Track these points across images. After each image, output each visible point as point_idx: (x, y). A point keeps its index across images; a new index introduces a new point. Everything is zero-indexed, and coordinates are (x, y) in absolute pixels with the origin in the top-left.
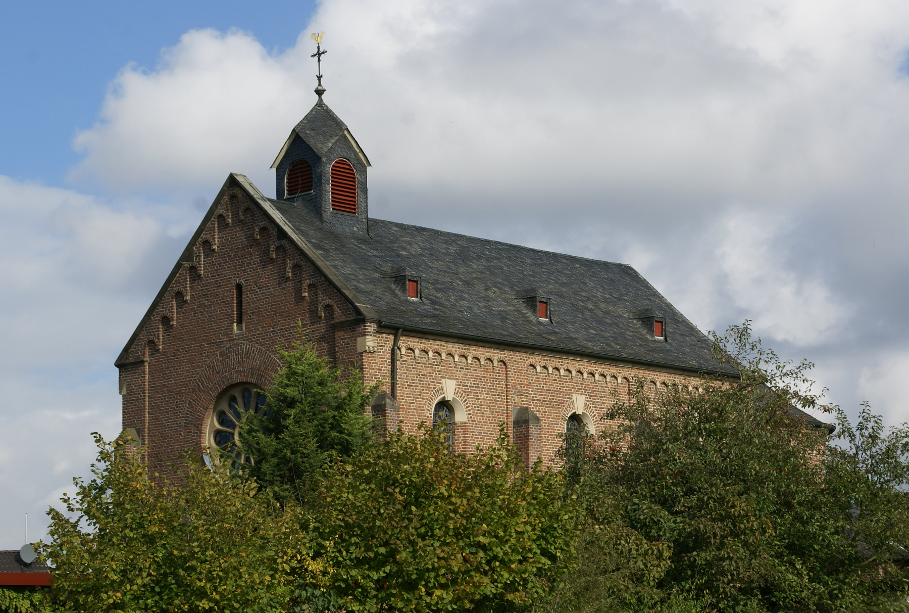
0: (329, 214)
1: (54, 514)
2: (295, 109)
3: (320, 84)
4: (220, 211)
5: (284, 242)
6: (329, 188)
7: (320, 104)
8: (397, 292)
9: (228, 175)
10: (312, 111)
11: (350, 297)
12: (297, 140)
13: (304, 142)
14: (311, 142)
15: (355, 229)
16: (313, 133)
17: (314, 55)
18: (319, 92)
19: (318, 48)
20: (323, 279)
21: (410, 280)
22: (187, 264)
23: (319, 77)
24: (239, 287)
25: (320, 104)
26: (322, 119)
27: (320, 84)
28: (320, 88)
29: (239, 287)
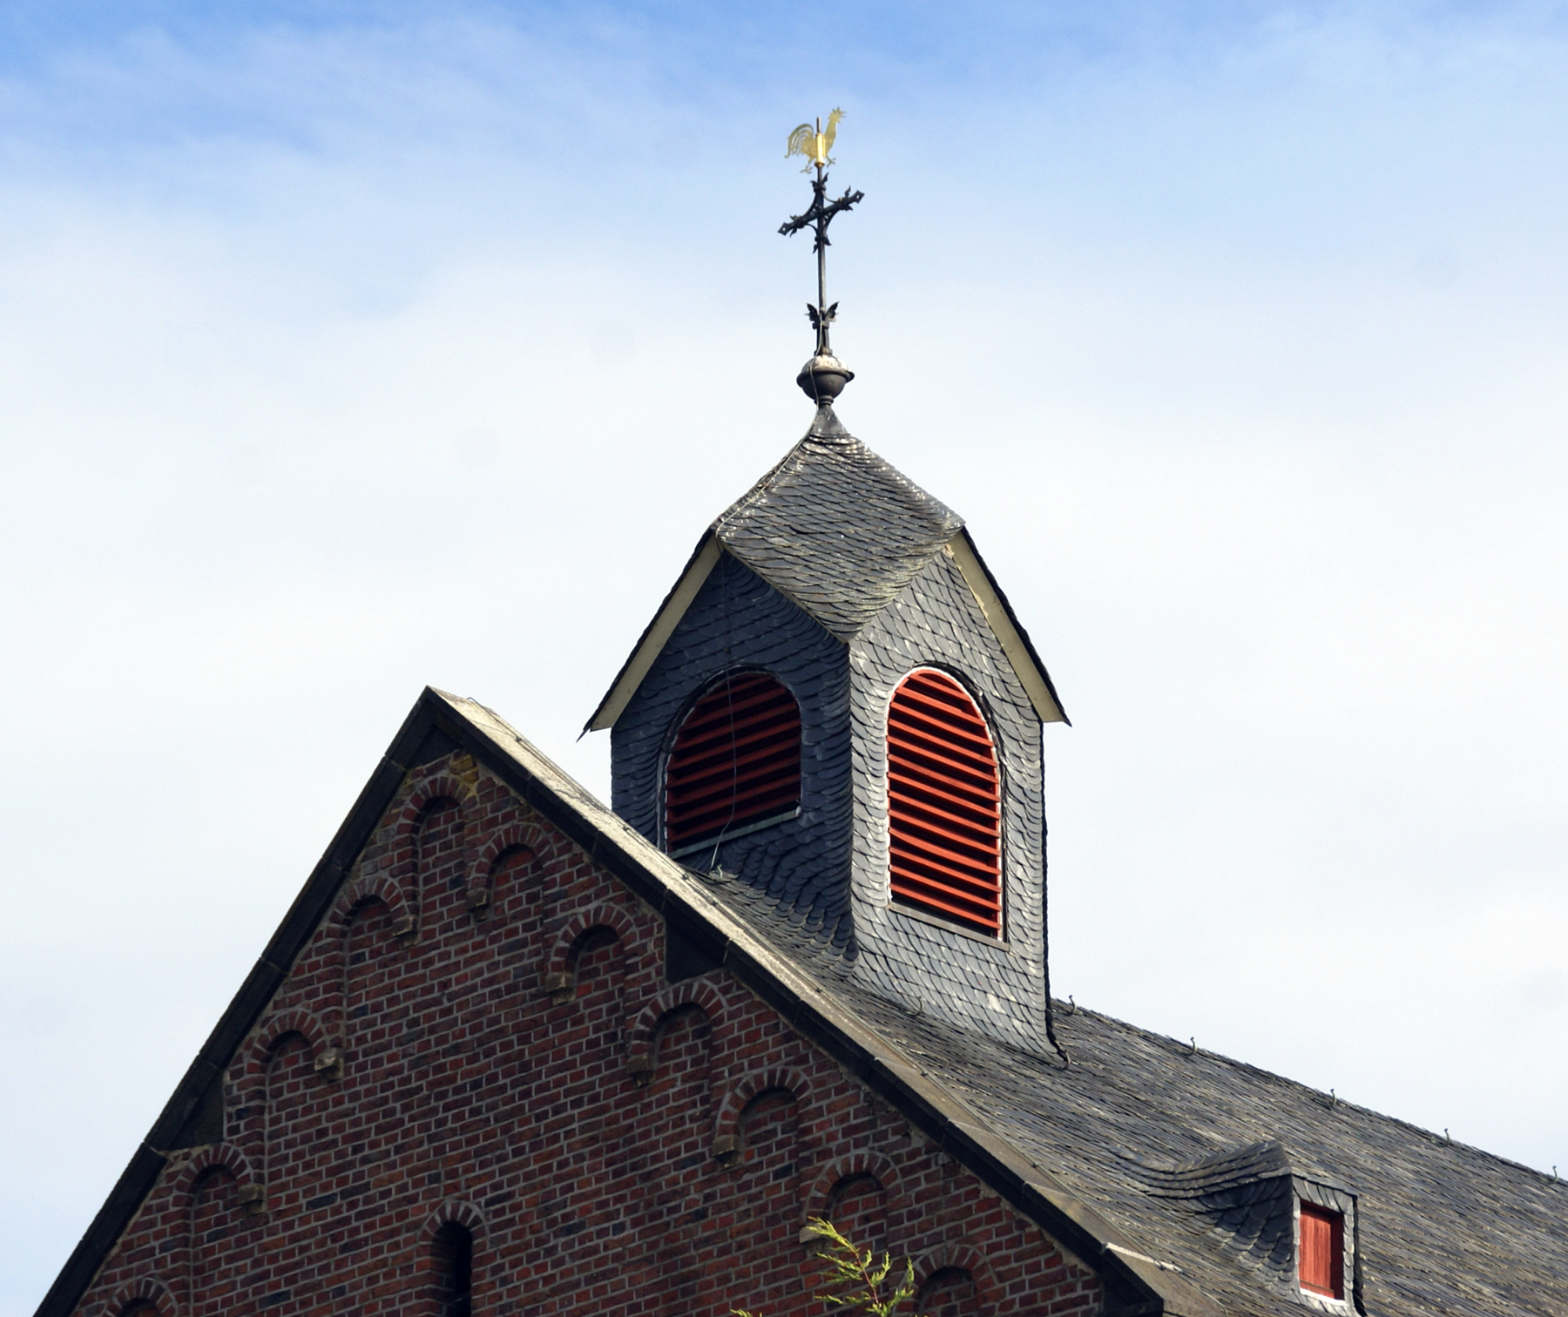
0: (880, 917)
1: (810, 307)
2: (722, 448)
3: (822, 347)
4: (366, 878)
5: (704, 984)
6: (874, 794)
7: (826, 435)
8: (1242, 1258)
9: (422, 690)
10: (788, 461)
11: (1073, 1213)
12: (723, 577)
13: (761, 584)
14: (798, 581)
15: (994, 1004)
16: (800, 547)
17: (799, 223)
18: (819, 385)
19: (819, 188)
20: (918, 1140)
21: (1308, 1207)
22: (183, 1162)
23: (820, 318)
24: (455, 1243)
25: (826, 435)
26: (841, 496)
27: (822, 347)
28: (824, 362)
29: (455, 1243)
